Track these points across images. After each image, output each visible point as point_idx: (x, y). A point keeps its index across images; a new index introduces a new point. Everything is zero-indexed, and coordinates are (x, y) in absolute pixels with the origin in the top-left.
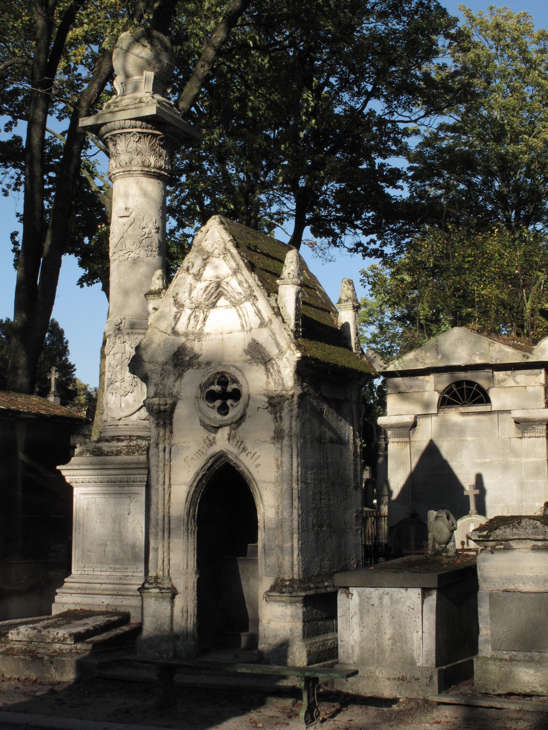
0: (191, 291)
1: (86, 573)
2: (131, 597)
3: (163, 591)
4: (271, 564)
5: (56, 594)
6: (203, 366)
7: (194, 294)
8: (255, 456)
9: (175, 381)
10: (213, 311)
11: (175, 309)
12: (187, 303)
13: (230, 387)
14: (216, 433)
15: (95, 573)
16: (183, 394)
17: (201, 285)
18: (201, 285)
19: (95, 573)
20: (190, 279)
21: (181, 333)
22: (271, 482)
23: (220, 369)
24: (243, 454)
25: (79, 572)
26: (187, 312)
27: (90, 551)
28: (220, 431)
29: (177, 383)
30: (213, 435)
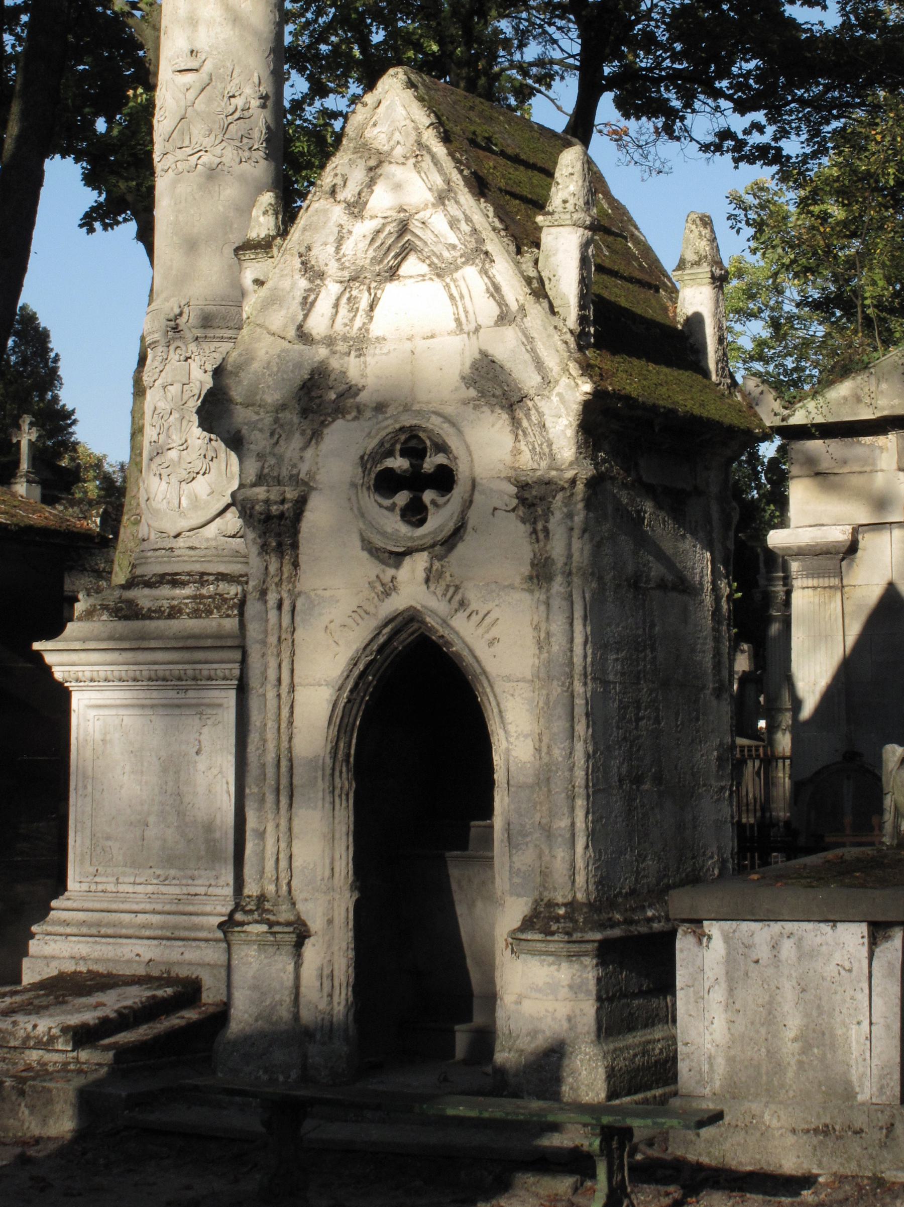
0: (340, 241)
1: (100, 887)
2: (202, 944)
3: (276, 929)
4: (524, 868)
5: (32, 936)
6: (368, 414)
7: (348, 247)
8: (488, 620)
9: (304, 448)
10: (391, 288)
11: (303, 283)
12: (332, 269)
13: (430, 463)
14: (397, 566)
15: (121, 888)
16: (322, 477)
17: (363, 228)
18: (363, 228)
19: (121, 888)
20: (337, 213)
21: (317, 337)
22: (524, 680)
23: (408, 421)
24: (459, 614)
25: (85, 887)
26: (331, 289)
27: (108, 838)
28: (407, 562)
29: (309, 453)
30: (391, 572)
